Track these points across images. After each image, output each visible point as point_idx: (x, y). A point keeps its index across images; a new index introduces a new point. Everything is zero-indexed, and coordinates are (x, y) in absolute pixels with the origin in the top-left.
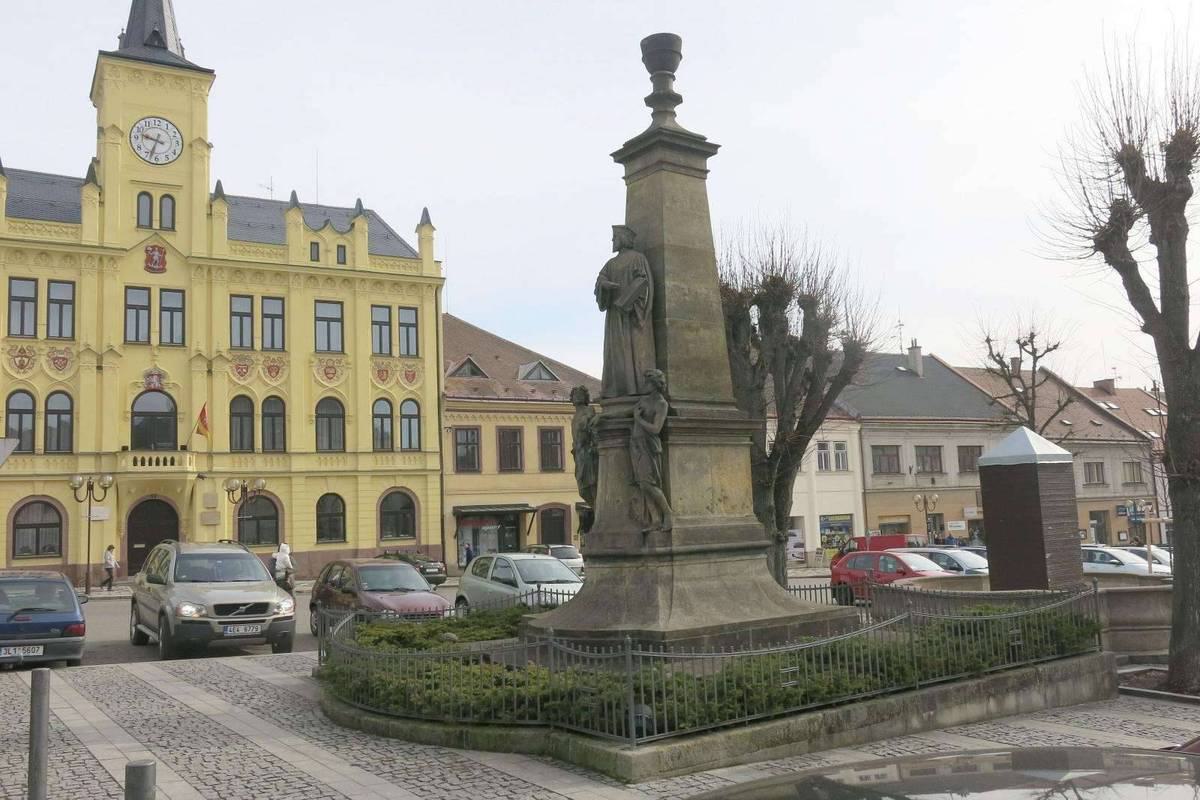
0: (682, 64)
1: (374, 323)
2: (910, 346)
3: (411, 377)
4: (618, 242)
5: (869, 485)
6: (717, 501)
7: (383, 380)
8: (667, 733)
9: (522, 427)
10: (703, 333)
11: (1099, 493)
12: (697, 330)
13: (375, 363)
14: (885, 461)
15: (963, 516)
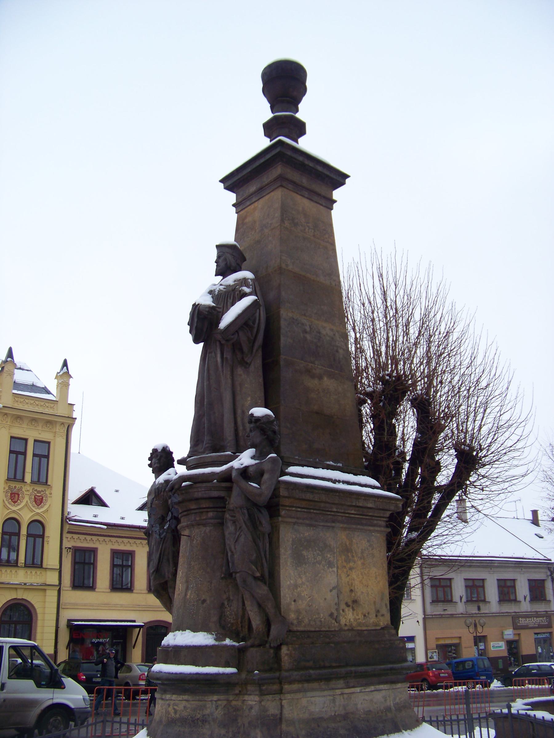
1: (11, 452)
3: (39, 501)
4: (222, 264)
6: (343, 606)
7: (15, 502)
9: (134, 551)
10: (327, 382)
12: (320, 378)
13: (9, 487)
15: (503, 638)
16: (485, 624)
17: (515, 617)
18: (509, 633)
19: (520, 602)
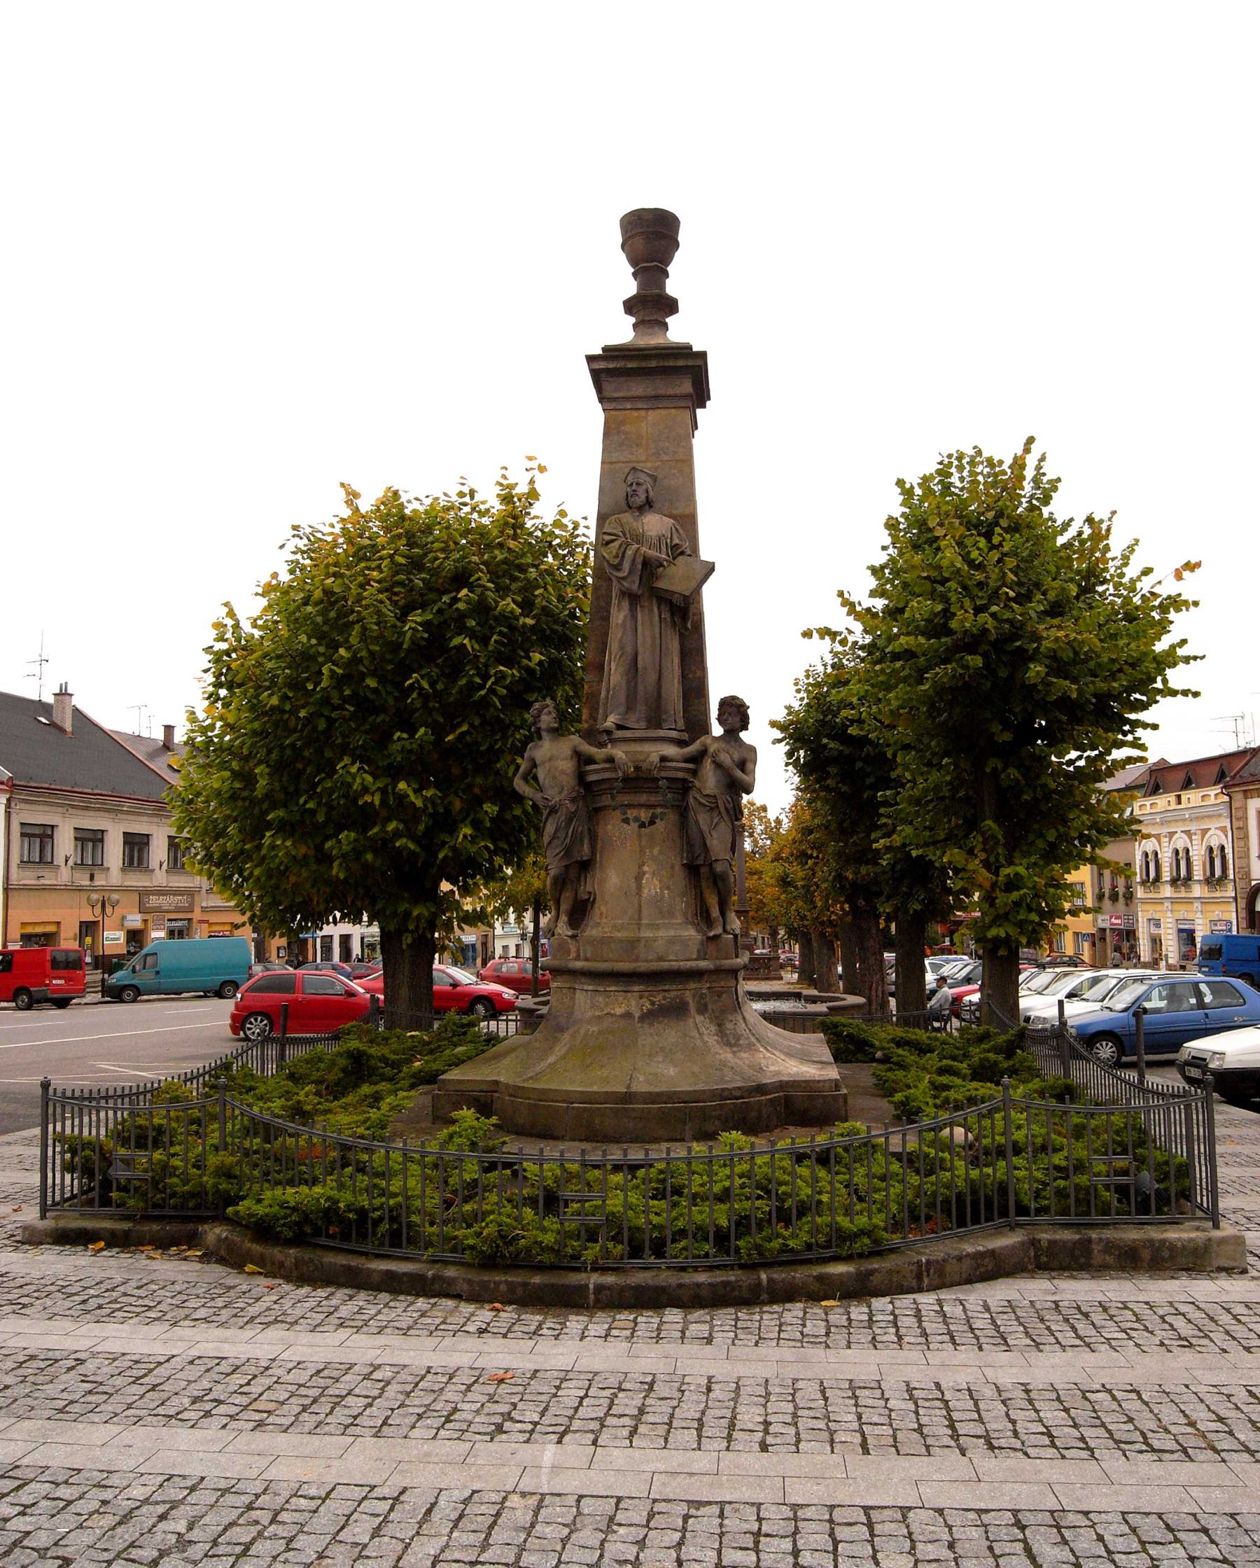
0: (678, 256)
2: (58, 691)
16: (118, 902)
17: (143, 894)
18: (135, 921)
19: (153, 871)
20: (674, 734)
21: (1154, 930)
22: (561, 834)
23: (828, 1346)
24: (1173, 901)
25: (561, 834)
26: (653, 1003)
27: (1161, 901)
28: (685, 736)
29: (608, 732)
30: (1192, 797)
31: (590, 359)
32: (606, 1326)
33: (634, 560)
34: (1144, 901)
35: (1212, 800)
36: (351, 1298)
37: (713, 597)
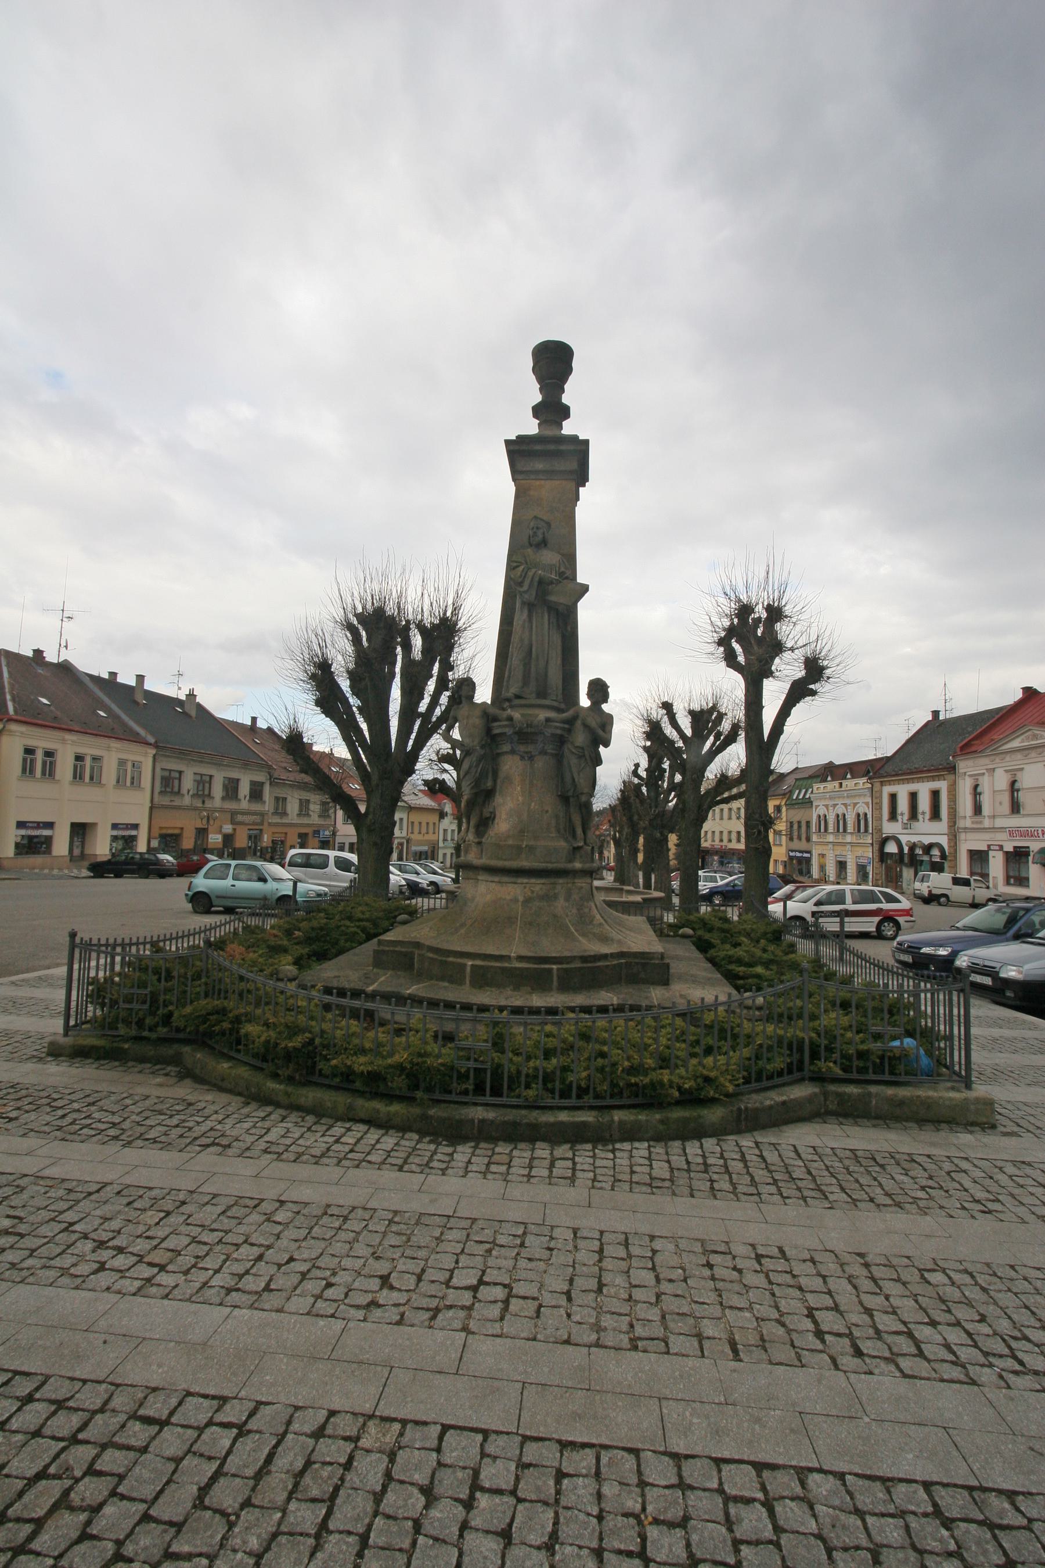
5: (157, 798)
8: (855, 1073)
11: (305, 821)
14: (169, 783)
17: (234, 814)
18: (228, 828)
20: (555, 704)
21: (822, 860)
22: (473, 770)
23: (674, 1194)
24: (834, 844)
25: (473, 770)
26: (533, 892)
27: (844, 844)
28: (563, 706)
29: (508, 700)
30: (849, 783)
31: (508, 443)
32: (486, 1160)
33: (533, 578)
34: (818, 843)
35: (861, 786)
36: (283, 1119)
37: (586, 612)
